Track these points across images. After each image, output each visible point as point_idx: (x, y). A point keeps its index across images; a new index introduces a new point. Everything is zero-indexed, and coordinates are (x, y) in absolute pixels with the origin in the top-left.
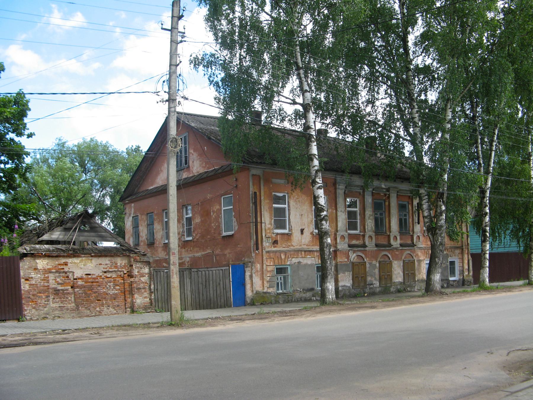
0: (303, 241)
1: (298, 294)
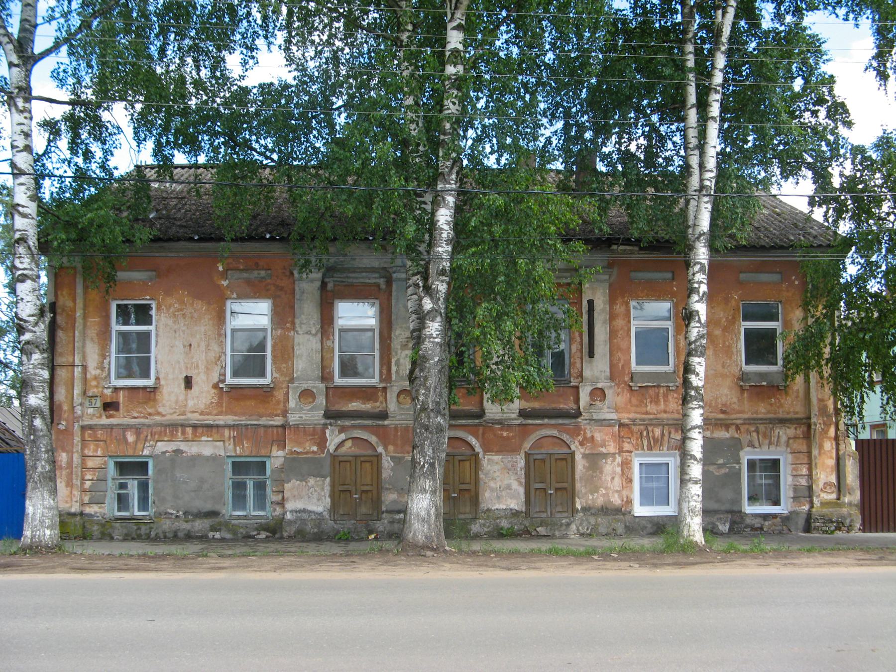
0: (191, 403)
1: (168, 522)
